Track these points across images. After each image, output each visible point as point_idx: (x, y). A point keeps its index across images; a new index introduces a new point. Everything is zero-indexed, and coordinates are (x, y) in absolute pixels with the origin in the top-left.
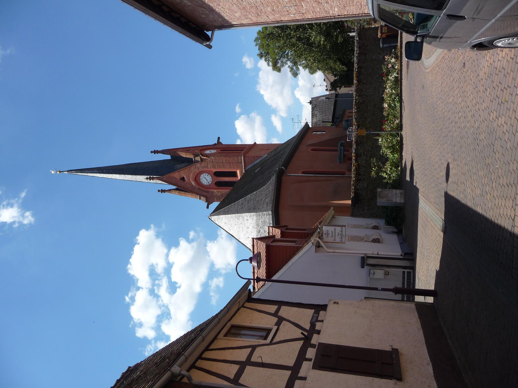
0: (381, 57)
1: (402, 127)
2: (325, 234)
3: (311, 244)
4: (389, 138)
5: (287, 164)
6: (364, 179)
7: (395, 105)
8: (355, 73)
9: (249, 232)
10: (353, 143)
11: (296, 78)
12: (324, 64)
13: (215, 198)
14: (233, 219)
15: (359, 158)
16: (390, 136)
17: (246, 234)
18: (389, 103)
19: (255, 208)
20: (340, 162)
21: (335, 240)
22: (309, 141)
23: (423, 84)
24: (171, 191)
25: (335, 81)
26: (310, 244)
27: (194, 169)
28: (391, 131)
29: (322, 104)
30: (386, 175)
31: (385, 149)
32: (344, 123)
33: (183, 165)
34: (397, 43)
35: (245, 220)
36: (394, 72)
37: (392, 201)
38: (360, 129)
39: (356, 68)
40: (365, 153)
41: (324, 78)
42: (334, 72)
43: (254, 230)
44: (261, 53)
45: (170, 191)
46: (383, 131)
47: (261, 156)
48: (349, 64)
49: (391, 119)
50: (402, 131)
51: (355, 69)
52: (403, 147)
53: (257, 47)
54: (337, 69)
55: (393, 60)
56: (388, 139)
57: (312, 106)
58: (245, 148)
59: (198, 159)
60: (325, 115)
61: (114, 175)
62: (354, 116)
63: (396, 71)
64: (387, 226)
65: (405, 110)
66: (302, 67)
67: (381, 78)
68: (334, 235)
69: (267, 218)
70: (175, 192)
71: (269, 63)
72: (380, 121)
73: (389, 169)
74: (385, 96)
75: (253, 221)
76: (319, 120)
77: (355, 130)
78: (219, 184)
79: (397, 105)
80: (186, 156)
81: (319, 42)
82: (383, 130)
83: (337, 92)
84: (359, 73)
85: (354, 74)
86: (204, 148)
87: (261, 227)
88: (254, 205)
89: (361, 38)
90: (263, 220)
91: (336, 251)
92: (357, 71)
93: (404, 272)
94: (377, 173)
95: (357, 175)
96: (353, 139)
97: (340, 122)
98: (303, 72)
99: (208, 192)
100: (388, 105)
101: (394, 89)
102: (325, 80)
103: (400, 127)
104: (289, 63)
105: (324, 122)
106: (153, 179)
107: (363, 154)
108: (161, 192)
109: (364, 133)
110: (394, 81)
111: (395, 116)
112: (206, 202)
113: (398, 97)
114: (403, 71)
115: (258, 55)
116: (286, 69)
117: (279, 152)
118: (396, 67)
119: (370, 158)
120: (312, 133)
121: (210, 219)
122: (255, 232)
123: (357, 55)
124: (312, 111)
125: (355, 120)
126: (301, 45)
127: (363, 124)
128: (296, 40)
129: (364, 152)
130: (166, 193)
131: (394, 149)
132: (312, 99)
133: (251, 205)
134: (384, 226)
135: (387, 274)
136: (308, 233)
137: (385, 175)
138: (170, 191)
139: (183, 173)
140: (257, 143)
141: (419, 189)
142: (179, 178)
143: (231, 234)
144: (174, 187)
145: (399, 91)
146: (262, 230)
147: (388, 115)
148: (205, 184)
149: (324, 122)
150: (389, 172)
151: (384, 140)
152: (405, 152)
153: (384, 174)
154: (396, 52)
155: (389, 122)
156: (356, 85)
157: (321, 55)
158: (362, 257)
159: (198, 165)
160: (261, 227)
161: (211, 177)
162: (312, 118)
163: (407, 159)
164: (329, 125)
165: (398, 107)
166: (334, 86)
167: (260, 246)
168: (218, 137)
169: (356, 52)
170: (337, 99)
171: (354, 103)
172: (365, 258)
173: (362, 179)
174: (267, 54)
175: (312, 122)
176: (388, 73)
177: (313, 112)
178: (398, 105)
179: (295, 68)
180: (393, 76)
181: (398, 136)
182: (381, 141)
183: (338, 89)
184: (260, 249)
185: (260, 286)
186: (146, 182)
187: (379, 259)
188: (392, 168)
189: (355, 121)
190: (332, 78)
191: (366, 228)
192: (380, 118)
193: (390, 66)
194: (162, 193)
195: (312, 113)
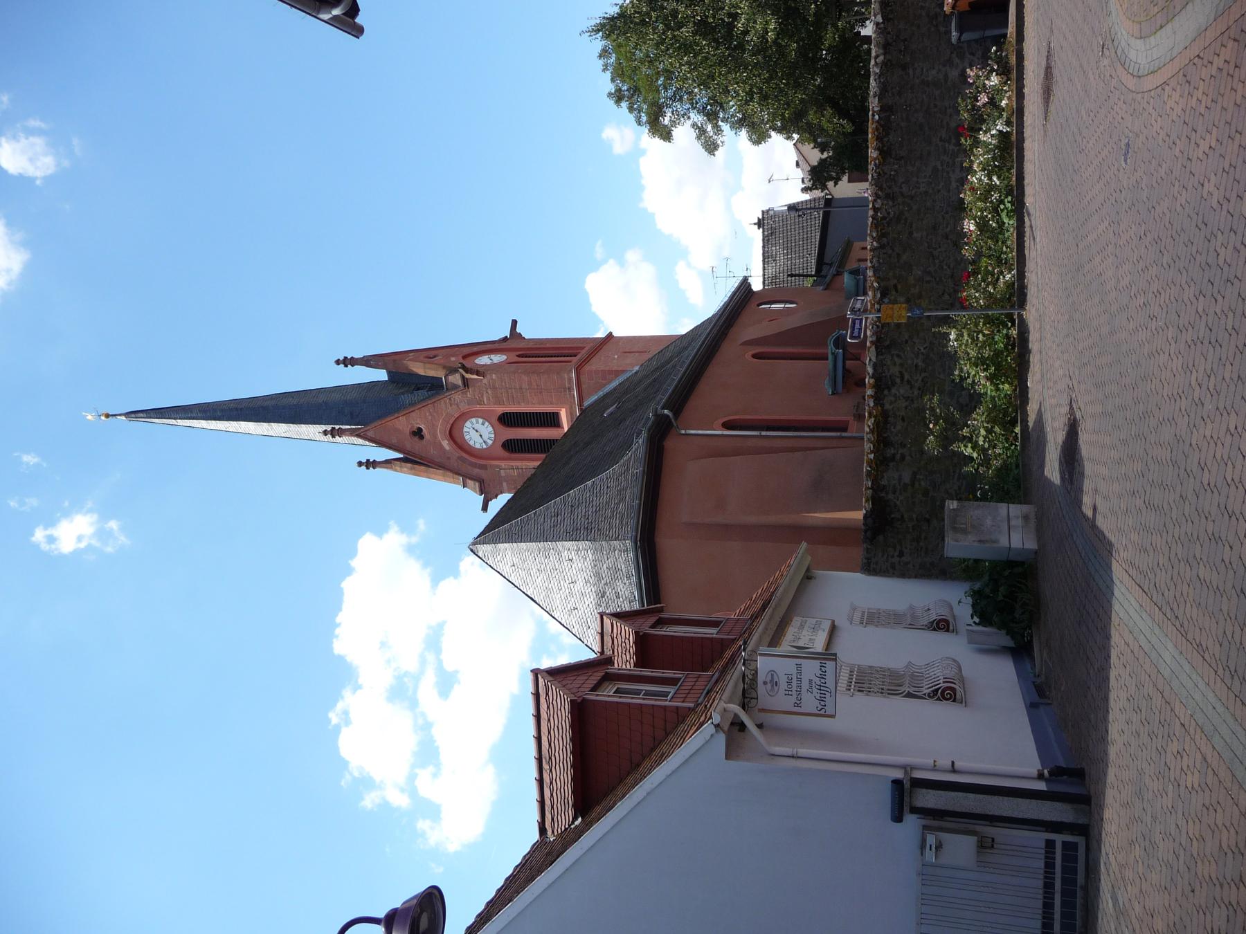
0: (954, 74)
1: (1025, 295)
2: (765, 683)
3: (712, 730)
4: (981, 331)
5: (679, 401)
6: (903, 457)
7: (1001, 224)
8: (871, 127)
9: (578, 595)
10: (868, 344)
11: (714, 155)
12: (780, 104)
13: (505, 484)
14: (533, 555)
15: (886, 392)
16: (984, 324)
17: (569, 599)
18: (982, 218)
19: (590, 528)
20: (833, 394)
21: (798, 705)
22: (750, 330)
23: (1125, 141)
24: (391, 463)
25: (822, 162)
26: (708, 729)
27: (446, 407)
28: (988, 307)
29: (789, 228)
30: (973, 448)
31: (968, 366)
32: (845, 280)
33: (422, 393)
34: (1007, 27)
35: (564, 561)
36: (998, 119)
37: (995, 545)
38: (889, 303)
39: (874, 112)
40: (906, 377)
41: (797, 159)
42: (819, 137)
43: (589, 590)
44: (619, 90)
45: (389, 465)
46: (964, 308)
47: (623, 372)
48: (858, 115)
49: (990, 268)
50: (1025, 309)
51: (873, 115)
52: (1029, 362)
53: (608, 75)
54: (825, 128)
55: (994, 80)
56: (978, 333)
57: (763, 231)
58: (583, 348)
59: (456, 379)
60: (797, 255)
61: (242, 423)
62: (871, 262)
63: (1005, 116)
64: (980, 628)
65: (1038, 240)
66: (728, 125)
67: (953, 141)
68: (794, 688)
69: (623, 558)
70: (401, 467)
71: (641, 116)
72: (952, 276)
73: (983, 432)
74: (967, 197)
75: (586, 563)
76: (781, 269)
77: (873, 305)
78: (512, 447)
79: (1007, 225)
80: (425, 372)
81: (763, 37)
82: (962, 305)
83: (830, 194)
84: (885, 127)
85: (870, 130)
86: (475, 349)
87: (608, 581)
88: (588, 518)
89: (891, 16)
90: (611, 562)
91: (803, 752)
92: (878, 122)
93: (1050, 844)
94: (946, 439)
95: (882, 445)
96: (869, 333)
97: (834, 275)
98: (735, 141)
99: (484, 467)
100: (977, 225)
101: (998, 171)
102: (800, 163)
103: (1018, 294)
104: (696, 117)
105: (792, 275)
106: (340, 433)
107: (898, 380)
108: (366, 466)
109: (900, 313)
110: (996, 147)
111: (999, 261)
112: (481, 495)
113: (1010, 198)
114: (1026, 114)
115: (610, 94)
116: (684, 133)
117: (668, 362)
118: (1004, 103)
119: (923, 392)
120: (759, 305)
121: (474, 553)
122: (591, 593)
123: (877, 71)
124: (764, 247)
125: (874, 272)
126: (708, 45)
127: (899, 287)
128: (695, 33)
129: (901, 373)
130: (379, 471)
131: (999, 367)
132: (763, 214)
133: (580, 517)
134: (970, 628)
135: (985, 845)
136: (722, 639)
137: (969, 450)
138: (388, 463)
139: (417, 419)
140: (615, 334)
141: (1108, 547)
142: (407, 431)
143: (529, 595)
144: (401, 456)
145: (1014, 179)
146: (610, 590)
147: (979, 254)
148: (478, 446)
149: (792, 275)
150: (984, 441)
151: (966, 337)
152: (1037, 377)
153: (966, 446)
154: (1001, 54)
155: (982, 277)
156: (875, 165)
157: (771, 78)
158: (897, 783)
159: (457, 397)
160: (608, 581)
161: (490, 429)
162: (764, 264)
163: (1046, 405)
164: (809, 282)
165: (1012, 230)
166: (818, 176)
167: (554, 702)
168: (513, 320)
169: (876, 62)
170: (830, 211)
171: (871, 219)
172: (907, 785)
173: (898, 457)
174: (635, 92)
175: (764, 275)
176: (979, 121)
177: (766, 249)
178: (1010, 222)
179: (709, 128)
180: (994, 132)
181: (1010, 324)
182: (956, 340)
183: (830, 184)
184: (556, 711)
185: (563, 829)
186: (326, 440)
187: (956, 793)
188: (992, 427)
189: (875, 275)
190: (815, 156)
191: (911, 626)
192: (952, 266)
193: (983, 99)
194: (368, 468)
195: (764, 251)
